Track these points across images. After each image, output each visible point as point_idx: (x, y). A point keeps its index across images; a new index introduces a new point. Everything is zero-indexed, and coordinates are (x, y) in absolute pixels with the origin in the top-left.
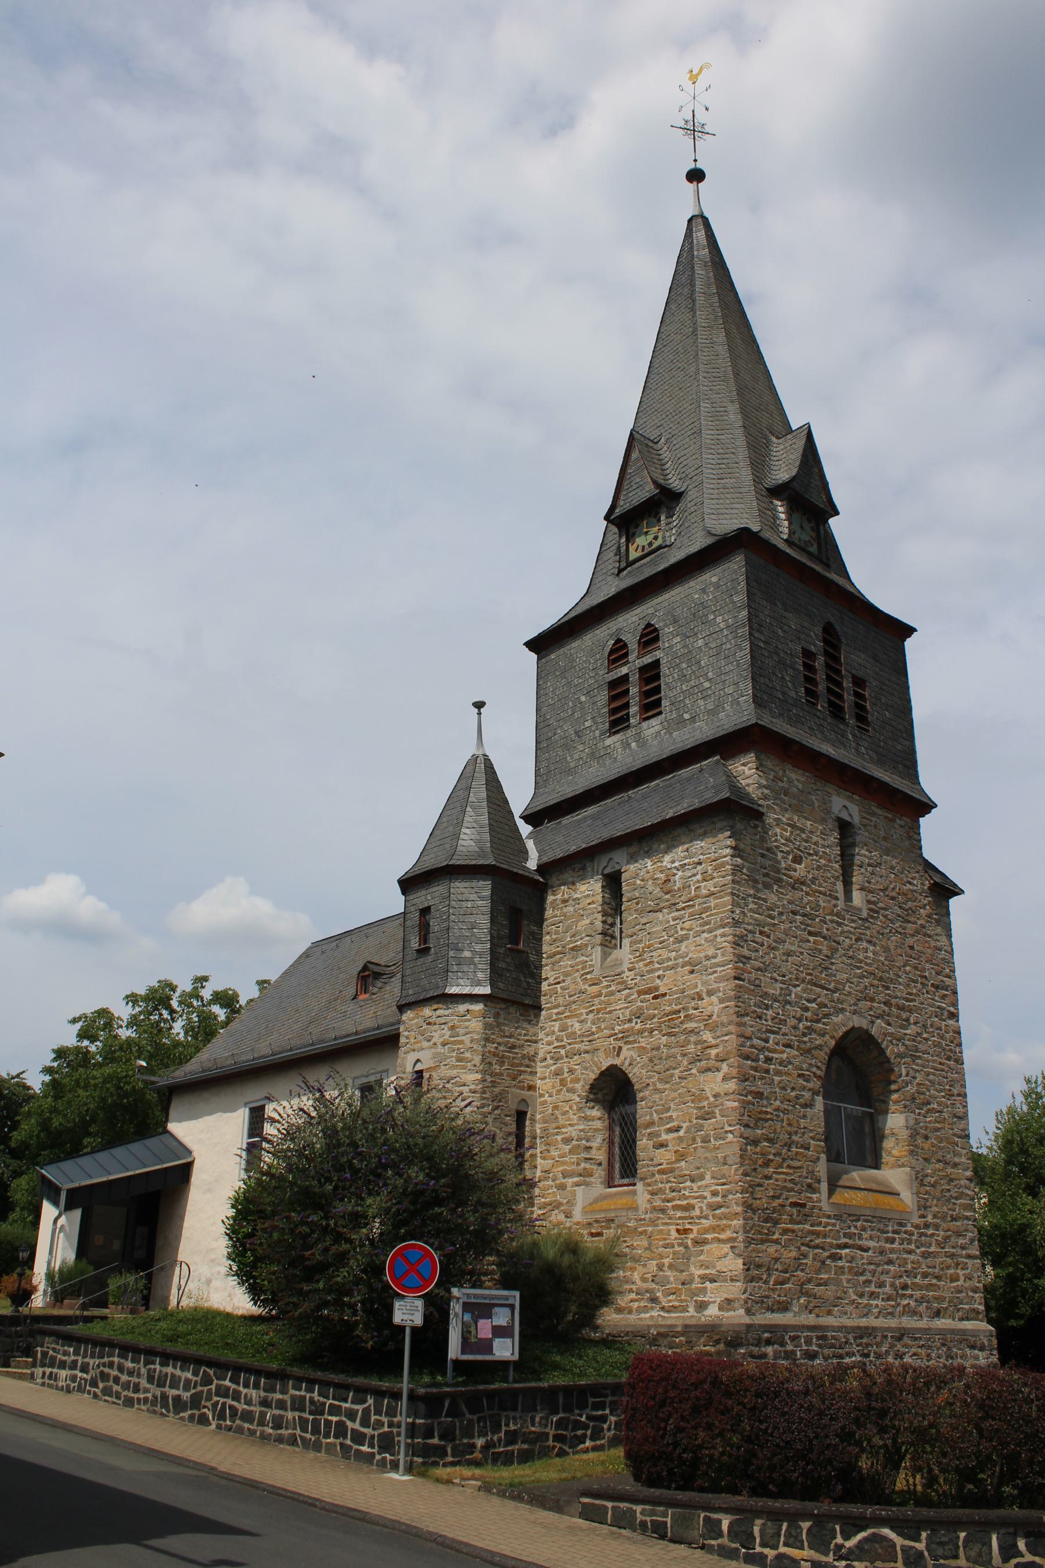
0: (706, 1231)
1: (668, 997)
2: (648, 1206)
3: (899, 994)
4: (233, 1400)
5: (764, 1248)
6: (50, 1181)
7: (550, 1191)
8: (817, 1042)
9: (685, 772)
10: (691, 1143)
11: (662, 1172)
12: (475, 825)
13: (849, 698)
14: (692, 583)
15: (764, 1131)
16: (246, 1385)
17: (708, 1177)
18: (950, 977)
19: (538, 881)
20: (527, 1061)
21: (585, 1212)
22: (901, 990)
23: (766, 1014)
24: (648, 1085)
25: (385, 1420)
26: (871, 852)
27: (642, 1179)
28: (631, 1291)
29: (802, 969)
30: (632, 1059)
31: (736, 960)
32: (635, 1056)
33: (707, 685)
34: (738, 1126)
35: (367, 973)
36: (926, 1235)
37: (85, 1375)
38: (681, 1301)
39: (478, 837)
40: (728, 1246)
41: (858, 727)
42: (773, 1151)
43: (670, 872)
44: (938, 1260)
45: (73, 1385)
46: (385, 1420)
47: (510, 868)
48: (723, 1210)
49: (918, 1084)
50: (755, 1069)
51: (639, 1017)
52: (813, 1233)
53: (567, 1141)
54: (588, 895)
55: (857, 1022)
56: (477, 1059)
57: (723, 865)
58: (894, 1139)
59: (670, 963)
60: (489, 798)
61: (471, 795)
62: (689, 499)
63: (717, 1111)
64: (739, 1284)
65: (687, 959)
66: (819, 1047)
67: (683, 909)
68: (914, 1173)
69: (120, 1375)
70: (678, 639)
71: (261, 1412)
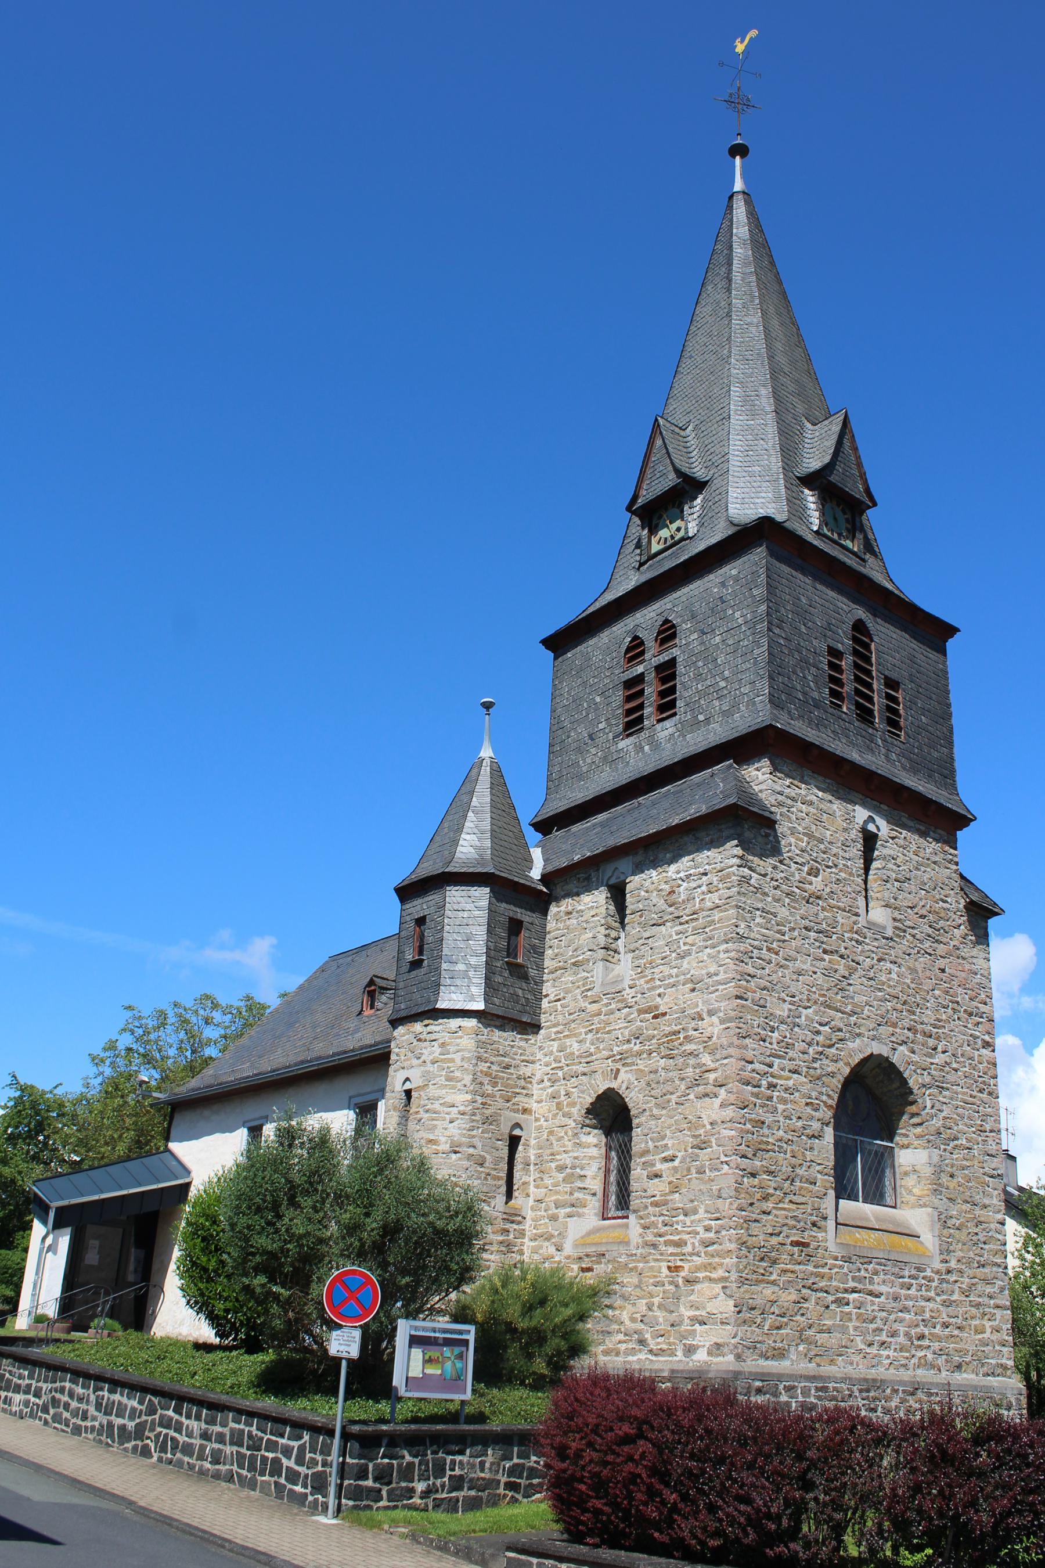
0: (698, 1269)
1: (667, 1017)
2: (640, 1241)
3: (926, 1020)
4: (175, 1431)
5: (760, 1289)
6: (41, 1199)
7: (542, 1222)
8: (829, 1069)
9: (696, 778)
10: (685, 1173)
11: (656, 1204)
12: (476, 831)
13: (878, 703)
14: (711, 577)
15: (764, 1163)
16: (188, 1417)
17: (701, 1211)
18: (985, 1003)
19: (541, 891)
20: (522, 1083)
21: (576, 1246)
22: (929, 1016)
23: (771, 1037)
24: (645, 1110)
25: (319, 1458)
26: (899, 866)
27: (635, 1211)
28: (619, 1331)
29: (814, 989)
30: (630, 1083)
31: (739, 977)
32: (633, 1079)
33: (723, 684)
34: (734, 1157)
35: (373, 988)
36: (948, 1282)
37: (37, 1401)
38: (670, 1344)
39: (478, 844)
40: (720, 1286)
41: (889, 731)
42: (773, 1184)
43: (674, 883)
44: (961, 1310)
45: (25, 1410)
46: (319, 1458)
47: (510, 877)
48: (715, 1246)
49: (945, 1118)
50: (756, 1095)
51: (638, 1038)
52: (817, 1275)
53: (561, 1168)
54: (592, 907)
55: (877, 1049)
56: (467, 1079)
57: (728, 876)
58: (915, 1177)
59: (672, 980)
60: (493, 805)
61: (474, 799)
62: (714, 488)
63: (714, 1141)
64: (728, 1327)
65: (689, 976)
66: (832, 1075)
67: (687, 922)
68: (936, 1214)
69: (70, 1401)
70: (695, 636)
71: (201, 1445)
